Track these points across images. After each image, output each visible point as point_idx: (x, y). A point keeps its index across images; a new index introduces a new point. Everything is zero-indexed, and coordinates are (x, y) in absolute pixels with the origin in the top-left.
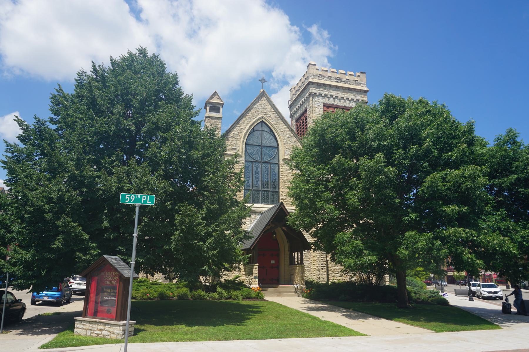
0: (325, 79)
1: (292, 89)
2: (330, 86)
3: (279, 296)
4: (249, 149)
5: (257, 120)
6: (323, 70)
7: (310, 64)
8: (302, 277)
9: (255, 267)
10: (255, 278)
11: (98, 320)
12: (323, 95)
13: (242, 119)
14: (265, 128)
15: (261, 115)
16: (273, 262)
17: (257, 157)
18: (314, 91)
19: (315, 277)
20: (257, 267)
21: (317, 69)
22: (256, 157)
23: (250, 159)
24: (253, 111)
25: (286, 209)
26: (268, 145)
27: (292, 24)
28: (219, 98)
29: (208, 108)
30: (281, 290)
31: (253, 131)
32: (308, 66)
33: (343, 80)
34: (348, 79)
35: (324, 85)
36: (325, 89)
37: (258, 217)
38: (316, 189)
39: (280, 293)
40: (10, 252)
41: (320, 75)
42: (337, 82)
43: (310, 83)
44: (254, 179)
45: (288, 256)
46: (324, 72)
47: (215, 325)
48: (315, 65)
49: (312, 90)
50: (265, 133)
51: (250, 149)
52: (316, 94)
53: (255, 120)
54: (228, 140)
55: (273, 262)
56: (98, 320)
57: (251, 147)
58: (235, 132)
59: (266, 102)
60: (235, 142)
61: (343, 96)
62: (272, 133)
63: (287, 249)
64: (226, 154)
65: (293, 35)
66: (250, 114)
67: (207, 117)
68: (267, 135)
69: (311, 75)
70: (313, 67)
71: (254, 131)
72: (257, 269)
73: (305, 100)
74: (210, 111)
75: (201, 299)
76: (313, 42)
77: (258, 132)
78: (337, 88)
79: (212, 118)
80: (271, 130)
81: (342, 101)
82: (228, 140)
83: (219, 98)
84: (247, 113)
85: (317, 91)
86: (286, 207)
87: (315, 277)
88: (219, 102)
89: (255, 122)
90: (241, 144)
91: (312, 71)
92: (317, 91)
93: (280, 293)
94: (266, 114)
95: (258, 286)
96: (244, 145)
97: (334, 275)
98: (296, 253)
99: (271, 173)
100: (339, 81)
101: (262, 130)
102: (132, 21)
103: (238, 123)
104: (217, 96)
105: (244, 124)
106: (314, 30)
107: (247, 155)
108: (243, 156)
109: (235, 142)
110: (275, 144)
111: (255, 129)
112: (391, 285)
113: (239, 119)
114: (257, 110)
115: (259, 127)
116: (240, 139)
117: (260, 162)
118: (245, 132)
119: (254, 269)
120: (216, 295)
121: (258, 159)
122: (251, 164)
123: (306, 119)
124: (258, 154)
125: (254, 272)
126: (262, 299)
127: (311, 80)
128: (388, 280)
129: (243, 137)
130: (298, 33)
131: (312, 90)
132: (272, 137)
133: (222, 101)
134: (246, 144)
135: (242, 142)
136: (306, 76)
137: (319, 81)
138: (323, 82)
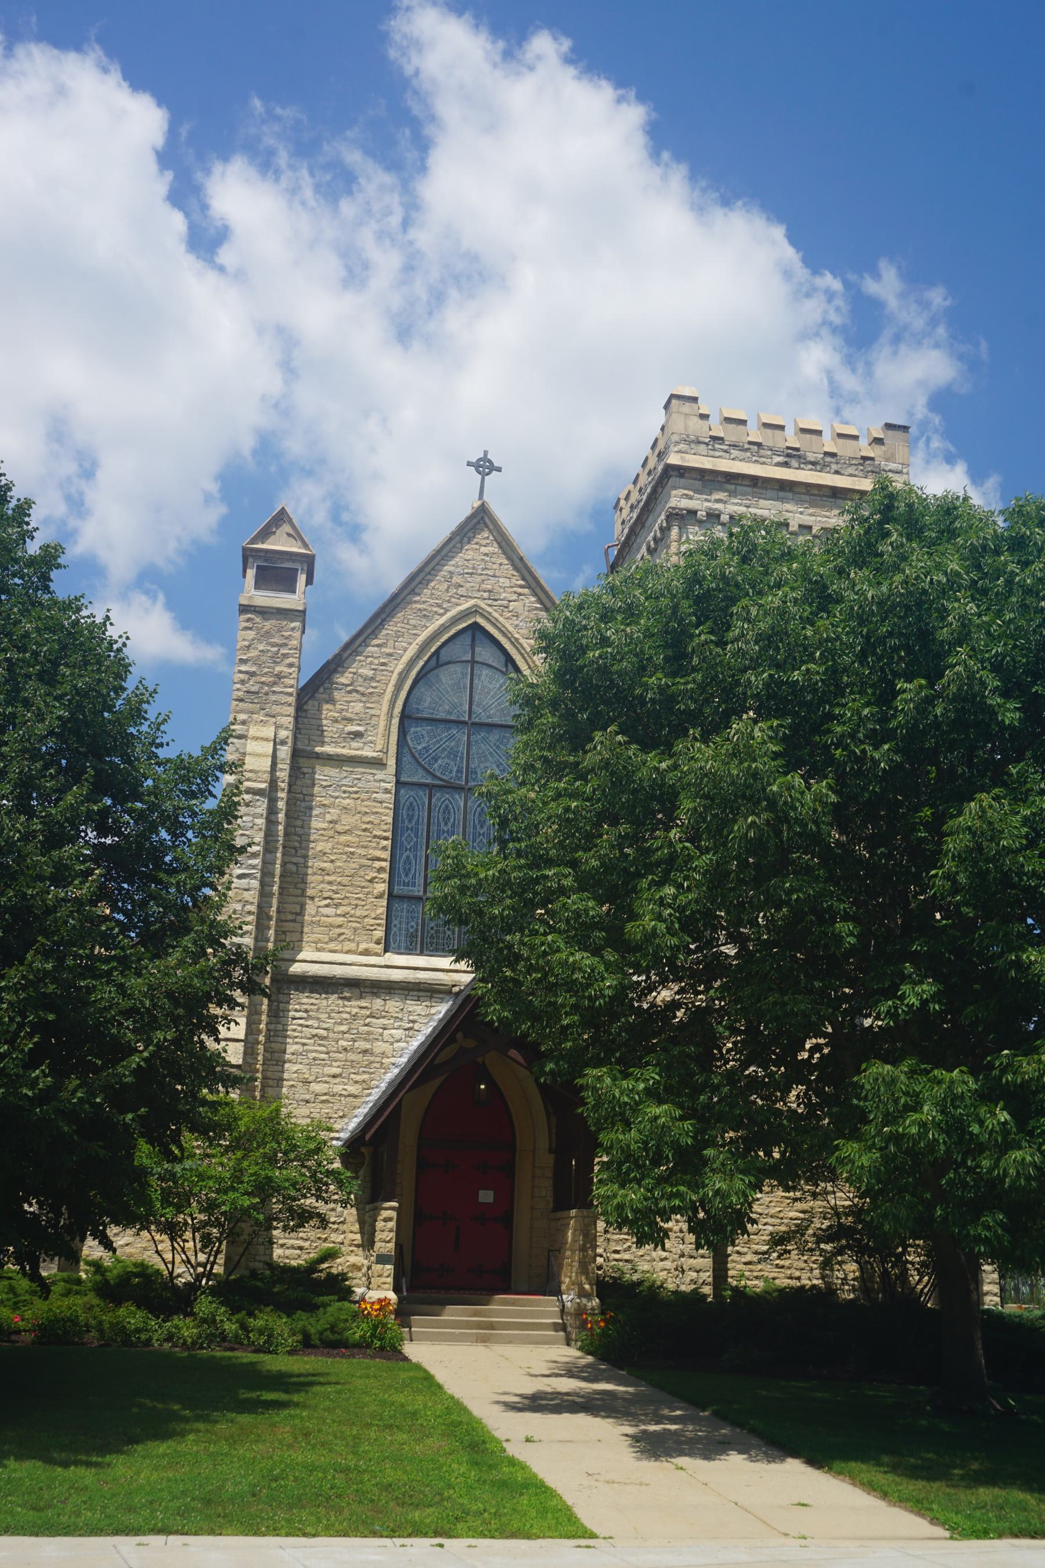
0: (735, 453)
1: (622, 503)
2: (755, 482)
3: (484, 1340)
4: (418, 738)
5: (454, 621)
6: (841, 436)
7: (673, 396)
8: (584, 1267)
9: (385, 1214)
10: (382, 1259)
13: (391, 615)
15: (472, 602)
16: (486, 1196)
17: (446, 768)
18: (685, 503)
19: (668, 1264)
20: (393, 1214)
21: (704, 417)
22: (445, 768)
23: (420, 777)
24: (438, 584)
26: (496, 720)
27: (814, 262)
28: (296, 535)
29: (251, 573)
30: (498, 1314)
31: (433, 664)
32: (667, 407)
33: (811, 457)
34: (833, 455)
35: (731, 480)
36: (733, 494)
37: (442, 1009)
38: (536, 881)
39: (491, 1326)
41: (714, 438)
42: (786, 464)
43: (669, 469)
46: (732, 427)
48: (695, 400)
49: (679, 499)
50: (485, 672)
51: (422, 737)
52: (693, 513)
53: (442, 620)
54: (332, 701)
55: (486, 1196)
57: (423, 730)
58: (361, 667)
59: (494, 548)
60: (358, 707)
63: (543, 1142)
64: (318, 756)
65: (813, 310)
66: (425, 598)
67: (244, 609)
69: (675, 438)
70: (687, 408)
71: (438, 665)
72: (392, 1224)
73: (655, 539)
74: (257, 587)
75: (127, 1342)
76: (887, 334)
77: (457, 668)
78: (785, 488)
79: (264, 612)
80: (509, 660)
82: (332, 701)
83: (296, 535)
84: (413, 592)
85: (700, 504)
87: (668, 1264)
88: (296, 548)
89: (443, 628)
90: (383, 717)
91: (686, 423)
92: (700, 504)
93: (491, 1326)
95: (392, 1296)
96: (396, 721)
97: (749, 1257)
99: (434, 828)
100: (794, 463)
101: (473, 662)
102: (188, 266)
103: (374, 634)
104: (286, 528)
105: (398, 635)
106: (886, 285)
107: (407, 759)
108: (392, 762)
109: (358, 707)
111: (444, 656)
112: (1011, 1308)
113: (377, 615)
114: (456, 579)
115: (460, 651)
116: (381, 695)
117: (459, 789)
118: (400, 667)
119: (380, 1225)
120: (187, 1329)
121: (450, 776)
122: (423, 795)
124: (453, 754)
125: (378, 1236)
126: (393, 1352)
127: (674, 459)
128: (996, 1289)
129: (390, 689)
130: (839, 302)
131: (679, 499)
133: (305, 545)
134: (404, 716)
135: (385, 707)
136: (660, 446)
137: (707, 463)
138: (725, 465)
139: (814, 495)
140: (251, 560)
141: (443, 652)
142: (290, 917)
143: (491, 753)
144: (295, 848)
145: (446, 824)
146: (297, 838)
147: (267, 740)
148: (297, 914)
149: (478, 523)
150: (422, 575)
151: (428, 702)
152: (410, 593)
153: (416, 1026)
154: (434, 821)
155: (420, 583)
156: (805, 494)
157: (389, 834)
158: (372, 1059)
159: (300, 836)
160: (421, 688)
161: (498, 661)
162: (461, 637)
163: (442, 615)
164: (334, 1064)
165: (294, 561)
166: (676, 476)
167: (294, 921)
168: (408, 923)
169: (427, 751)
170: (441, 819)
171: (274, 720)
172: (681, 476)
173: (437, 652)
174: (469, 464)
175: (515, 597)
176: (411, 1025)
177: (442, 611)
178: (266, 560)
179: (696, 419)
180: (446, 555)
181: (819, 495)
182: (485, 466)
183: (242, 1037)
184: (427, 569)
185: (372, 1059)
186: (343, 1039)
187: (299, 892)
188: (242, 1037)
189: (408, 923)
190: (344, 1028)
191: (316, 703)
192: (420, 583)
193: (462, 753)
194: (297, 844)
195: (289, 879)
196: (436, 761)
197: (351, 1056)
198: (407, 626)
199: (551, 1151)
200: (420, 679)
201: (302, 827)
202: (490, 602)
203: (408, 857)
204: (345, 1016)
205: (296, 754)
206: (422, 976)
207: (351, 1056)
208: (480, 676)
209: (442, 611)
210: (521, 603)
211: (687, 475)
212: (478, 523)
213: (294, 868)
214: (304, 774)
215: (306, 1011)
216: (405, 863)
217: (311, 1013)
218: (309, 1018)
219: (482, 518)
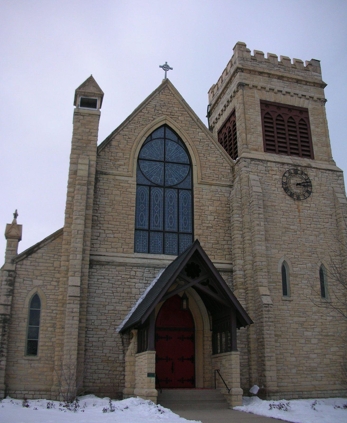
11: (219, 342)
12: (259, 88)
14: (169, 135)
23: (146, 182)
25: (212, 264)
40: (3, 287)
44: (152, 213)
45: (210, 339)
47: (176, 414)
56: (219, 342)
61: (289, 90)
62: (180, 142)
63: (207, 327)
68: (172, 146)
71: (151, 140)
80: (179, 138)
81: (279, 94)
86: (212, 261)
94: (172, 115)
98: (223, 335)
110: (186, 160)
121: (159, 182)
123: (235, 125)
132: (181, 149)
134: (139, 159)
139: (290, 82)
140: (78, 96)
141: (153, 135)
142: (96, 238)
143: (173, 174)
144: (96, 210)
145: (157, 201)
146: (98, 206)
147: (86, 164)
148: (98, 237)
149: (165, 87)
150: (145, 105)
151: (143, 155)
152: (140, 112)
153: (149, 282)
154: (152, 200)
155: (144, 108)
156: (287, 81)
157: (135, 205)
158: (131, 295)
159: (98, 205)
160: (145, 148)
161: (176, 139)
162: (160, 130)
163: (152, 120)
164: (116, 297)
165: (96, 96)
166: (241, 72)
167: (97, 239)
168: (143, 241)
169: (180, 152)
170: (155, 200)
171: (88, 157)
172: (242, 72)
173: (151, 135)
174: (160, 67)
175: (181, 115)
176: (147, 281)
177: (152, 119)
178: (84, 96)
179: (246, 53)
180: (154, 98)
181: (292, 82)
182: (166, 67)
183: (79, 285)
184: (147, 103)
185: (131, 295)
186: (119, 287)
187: (99, 228)
188: (79, 285)
189: (143, 241)
190: (119, 283)
191: (104, 153)
192: (144, 108)
193: (162, 174)
194: (97, 208)
195: (95, 222)
196: (152, 177)
197: (122, 295)
198: (139, 124)
199: (211, 330)
200: (145, 144)
201: (99, 201)
202: (171, 116)
203: (142, 214)
204: (119, 278)
205: (97, 172)
206: (152, 261)
207: (122, 295)
208: (168, 144)
209: (152, 119)
210: (183, 117)
211: (244, 71)
212: (165, 87)
213: (96, 218)
214: (100, 180)
215: (104, 276)
216: (141, 217)
217: (105, 277)
218: (105, 278)
219: (167, 86)
